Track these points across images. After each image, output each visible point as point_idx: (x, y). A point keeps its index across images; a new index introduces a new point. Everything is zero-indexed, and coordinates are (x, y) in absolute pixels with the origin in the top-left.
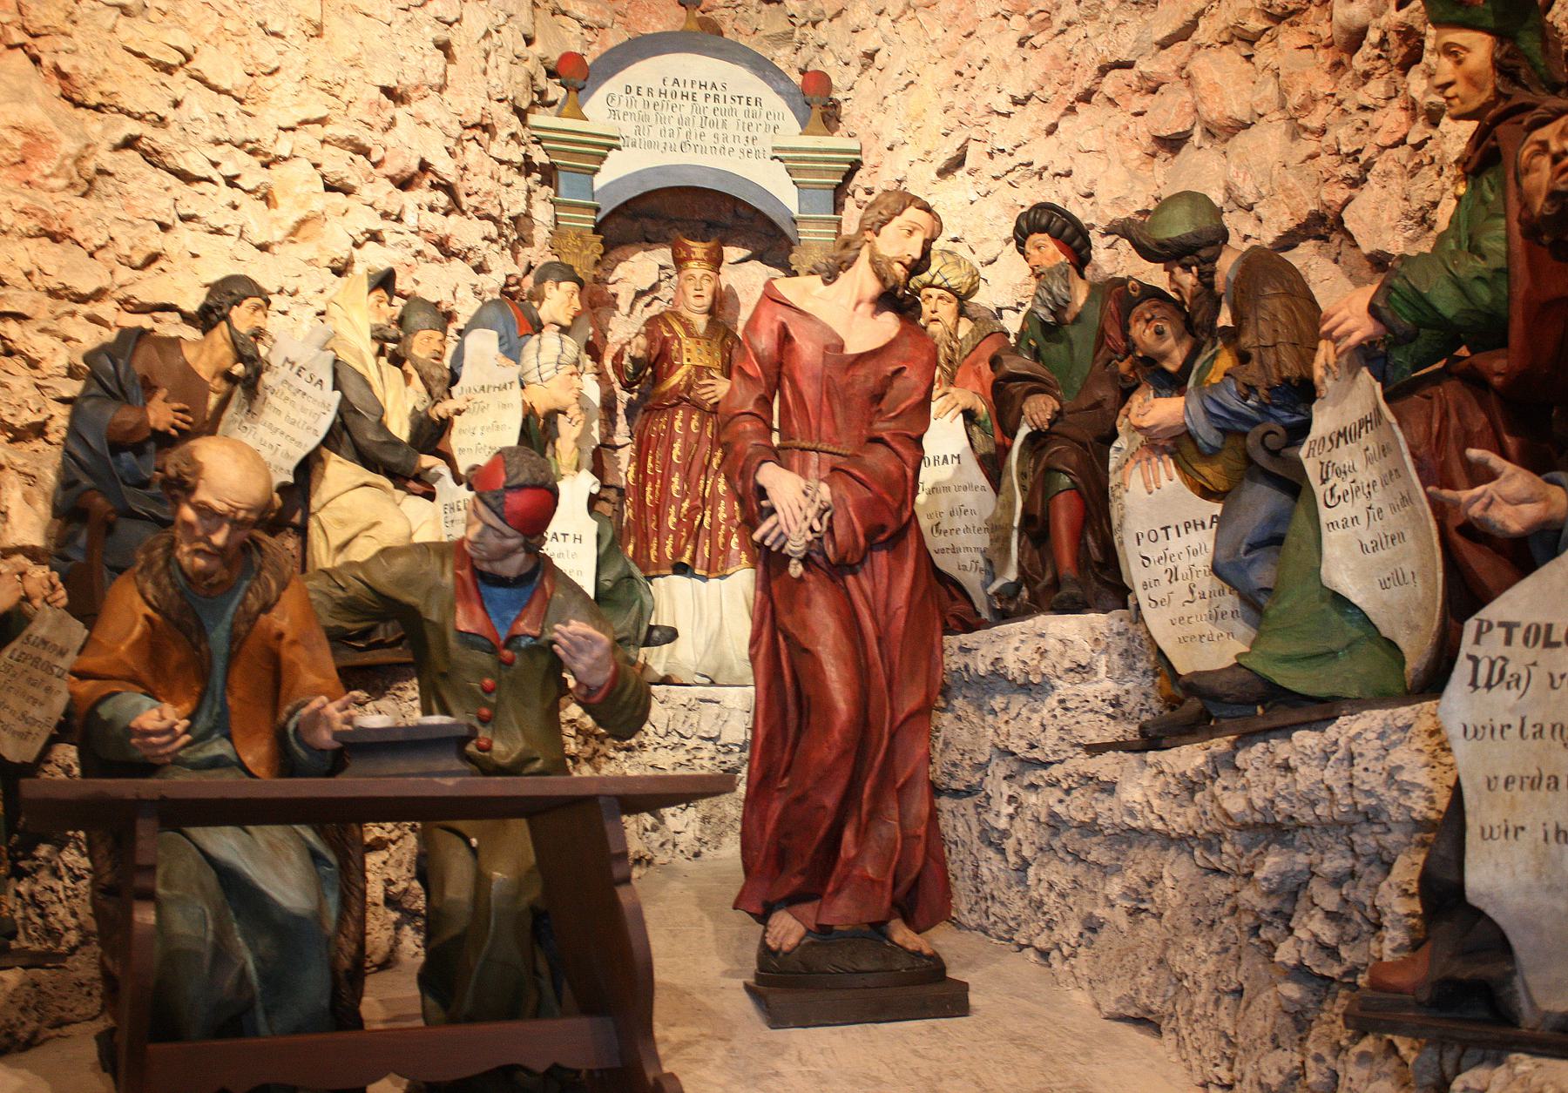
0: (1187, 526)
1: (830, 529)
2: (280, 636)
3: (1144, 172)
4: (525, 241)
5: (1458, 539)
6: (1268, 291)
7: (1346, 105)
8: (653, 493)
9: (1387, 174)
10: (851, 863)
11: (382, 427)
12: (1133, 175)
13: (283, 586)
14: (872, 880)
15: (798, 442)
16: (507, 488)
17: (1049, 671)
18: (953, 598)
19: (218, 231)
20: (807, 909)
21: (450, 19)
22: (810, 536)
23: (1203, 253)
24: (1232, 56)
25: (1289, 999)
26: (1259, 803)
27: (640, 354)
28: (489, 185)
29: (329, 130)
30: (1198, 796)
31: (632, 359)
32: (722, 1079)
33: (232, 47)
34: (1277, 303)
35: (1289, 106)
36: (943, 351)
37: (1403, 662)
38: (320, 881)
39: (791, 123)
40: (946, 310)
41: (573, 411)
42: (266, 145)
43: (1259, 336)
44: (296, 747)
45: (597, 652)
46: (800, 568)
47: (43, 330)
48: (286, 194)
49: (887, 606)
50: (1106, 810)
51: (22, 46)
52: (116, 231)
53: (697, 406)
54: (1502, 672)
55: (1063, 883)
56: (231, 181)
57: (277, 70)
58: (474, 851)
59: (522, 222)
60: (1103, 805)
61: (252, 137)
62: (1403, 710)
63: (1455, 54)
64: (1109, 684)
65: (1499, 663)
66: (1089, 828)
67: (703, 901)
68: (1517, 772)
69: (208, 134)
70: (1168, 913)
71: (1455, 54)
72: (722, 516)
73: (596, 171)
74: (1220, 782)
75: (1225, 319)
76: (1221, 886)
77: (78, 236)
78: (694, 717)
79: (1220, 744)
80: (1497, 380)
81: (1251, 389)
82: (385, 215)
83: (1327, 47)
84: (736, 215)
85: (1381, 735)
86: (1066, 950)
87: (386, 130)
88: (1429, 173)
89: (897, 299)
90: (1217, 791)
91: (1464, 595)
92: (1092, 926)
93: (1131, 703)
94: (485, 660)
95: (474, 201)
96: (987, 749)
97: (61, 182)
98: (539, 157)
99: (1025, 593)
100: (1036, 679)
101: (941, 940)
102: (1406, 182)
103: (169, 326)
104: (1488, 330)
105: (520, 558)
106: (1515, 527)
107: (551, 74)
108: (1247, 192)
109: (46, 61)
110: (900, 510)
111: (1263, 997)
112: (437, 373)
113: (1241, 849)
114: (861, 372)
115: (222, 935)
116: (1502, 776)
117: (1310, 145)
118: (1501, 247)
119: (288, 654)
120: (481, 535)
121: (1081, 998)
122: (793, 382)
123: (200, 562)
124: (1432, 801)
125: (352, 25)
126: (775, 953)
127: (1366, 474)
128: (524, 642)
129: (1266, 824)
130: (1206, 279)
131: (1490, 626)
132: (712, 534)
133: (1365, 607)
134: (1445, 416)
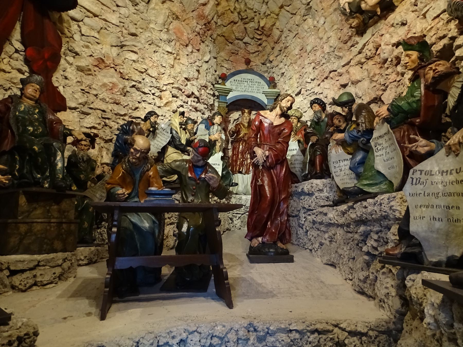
0: (344, 160)
2: (150, 176)
6: (364, 111)
7: (383, 75)
9: (391, 88)
10: (269, 229)
12: (336, 93)
13: (151, 166)
17: (313, 191)
19: (150, 104)
21: (200, 66)
23: (350, 104)
24: (358, 67)
25: (366, 260)
26: (359, 215)
28: (206, 98)
29: (174, 85)
30: (345, 215)
31: (232, 131)
33: (155, 69)
36: (294, 129)
37: (393, 186)
40: (295, 121)
41: (219, 140)
47: (113, 121)
48: (164, 97)
50: (325, 219)
51: (113, 67)
52: (129, 103)
54: (419, 181)
55: (315, 235)
56: (153, 94)
57: (164, 73)
59: (212, 105)
61: (158, 86)
62: (393, 193)
63: (409, 56)
64: (326, 194)
66: (321, 223)
68: (424, 204)
69: (149, 85)
70: (338, 241)
71: (409, 56)
74: (350, 211)
75: (354, 119)
76: (350, 235)
77: (122, 103)
79: (350, 204)
82: (184, 102)
84: (255, 105)
85: (388, 199)
86: (316, 249)
87: (185, 86)
89: (284, 115)
90: (349, 213)
91: (407, 168)
92: (321, 244)
93: (331, 198)
94: (193, 182)
95: (203, 101)
97: (119, 93)
98: (217, 94)
99: (309, 176)
101: (289, 247)
104: (416, 113)
105: (202, 162)
107: (220, 78)
108: (360, 94)
109: (118, 70)
111: (359, 259)
113: (354, 226)
117: (374, 84)
119: (151, 180)
121: (319, 260)
123: (134, 160)
124: (401, 213)
125: (180, 66)
126: (252, 247)
127: (385, 145)
130: (350, 110)
131: (416, 171)
133: (385, 174)
134: (404, 132)
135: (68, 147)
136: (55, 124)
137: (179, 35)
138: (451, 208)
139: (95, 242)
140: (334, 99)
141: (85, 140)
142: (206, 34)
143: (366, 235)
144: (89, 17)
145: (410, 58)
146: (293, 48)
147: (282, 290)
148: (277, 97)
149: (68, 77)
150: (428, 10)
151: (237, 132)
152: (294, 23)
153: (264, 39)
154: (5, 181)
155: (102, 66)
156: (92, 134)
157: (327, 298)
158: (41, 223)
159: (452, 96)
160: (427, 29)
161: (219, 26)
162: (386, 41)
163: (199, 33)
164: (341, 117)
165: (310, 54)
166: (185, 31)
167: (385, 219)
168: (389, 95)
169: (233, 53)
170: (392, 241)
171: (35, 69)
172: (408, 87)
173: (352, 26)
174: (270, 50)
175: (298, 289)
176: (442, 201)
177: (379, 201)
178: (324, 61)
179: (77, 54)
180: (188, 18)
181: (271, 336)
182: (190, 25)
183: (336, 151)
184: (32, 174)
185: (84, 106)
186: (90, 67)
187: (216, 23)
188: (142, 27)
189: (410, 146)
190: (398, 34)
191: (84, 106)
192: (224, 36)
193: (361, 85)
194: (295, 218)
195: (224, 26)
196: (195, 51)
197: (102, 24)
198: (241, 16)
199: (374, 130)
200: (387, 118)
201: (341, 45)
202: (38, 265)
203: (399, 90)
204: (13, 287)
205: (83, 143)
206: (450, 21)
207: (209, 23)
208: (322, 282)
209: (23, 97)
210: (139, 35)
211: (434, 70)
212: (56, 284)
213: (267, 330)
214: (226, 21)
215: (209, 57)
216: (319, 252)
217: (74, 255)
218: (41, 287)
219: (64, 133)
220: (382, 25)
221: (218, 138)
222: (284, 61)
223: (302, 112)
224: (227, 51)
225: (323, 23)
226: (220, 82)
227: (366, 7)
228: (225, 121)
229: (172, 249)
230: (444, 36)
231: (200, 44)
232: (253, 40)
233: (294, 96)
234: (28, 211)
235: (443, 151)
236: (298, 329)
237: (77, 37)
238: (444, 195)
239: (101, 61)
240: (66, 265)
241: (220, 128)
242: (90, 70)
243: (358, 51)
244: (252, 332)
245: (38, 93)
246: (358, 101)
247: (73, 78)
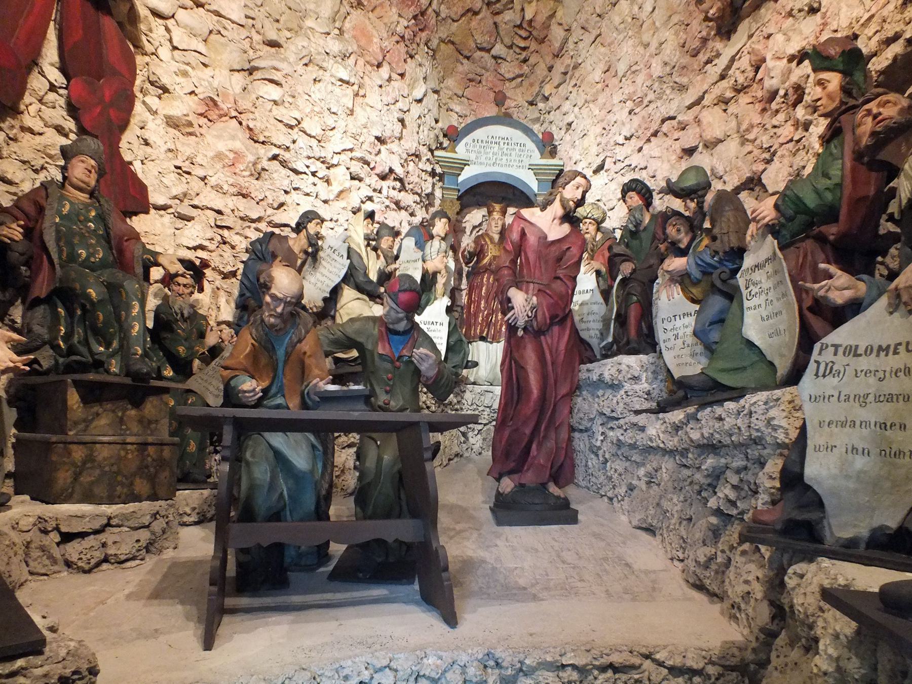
0: (684, 315)
1: (536, 316)
2: (305, 353)
4: (431, 204)
6: (727, 208)
9: (783, 156)
10: (534, 457)
11: (366, 275)
12: (672, 167)
13: (307, 332)
15: (526, 279)
17: (621, 379)
18: (586, 350)
19: (307, 194)
20: (516, 476)
21: (405, 110)
22: (527, 319)
23: (700, 193)
24: (718, 110)
25: (712, 524)
26: (706, 435)
27: (472, 250)
28: (417, 180)
29: (354, 154)
30: (680, 432)
32: (474, 547)
34: (730, 213)
35: (741, 130)
36: (590, 246)
38: (314, 457)
39: (537, 153)
40: (592, 228)
41: (443, 272)
42: (328, 159)
43: (721, 229)
44: (308, 400)
45: (431, 361)
47: (237, 234)
48: (335, 180)
49: (557, 350)
50: (641, 439)
51: (235, 117)
52: (267, 194)
55: (621, 469)
56: (314, 174)
58: (378, 446)
59: (430, 196)
61: (323, 155)
62: (776, 391)
64: (646, 385)
65: (830, 365)
66: (633, 446)
67: (480, 472)
68: (835, 418)
69: (305, 154)
70: (662, 484)
73: (459, 175)
74: (690, 426)
75: (707, 225)
76: (686, 472)
78: (483, 398)
79: (691, 410)
80: (832, 238)
81: (716, 252)
82: (375, 190)
83: (760, 102)
84: (514, 195)
85: (766, 403)
86: (620, 498)
87: (376, 155)
88: (802, 153)
89: (569, 218)
90: (688, 430)
91: (807, 340)
92: (631, 488)
93: (655, 394)
94: (388, 366)
95: (411, 186)
96: (595, 412)
97: (248, 173)
98: (439, 170)
99: (615, 347)
100: (616, 382)
101: (571, 492)
102: (791, 159)
103: (286, 232)
104: (830, 214)
106: (840, 301)
107: (445, 136)
108: (720, 170)
109: (244, 123)
110: (565, 308)
111: (701, 522)
112: (390, 255)
113: (696, 456)
114: (553, 249)
115: (273, 478)
116: (827, 421)
117: (749, 147)
118: (839, 173)
119: (308, 361)
120: (388, 312)
121: (624, 518)
123: (272, 320)
124: (787, 434)
125: (365, 110)
128: (405, 359)
129: (708, 445)
130: (700, 205)
131: (827, 346)
132: (495, 325)
133: (761, 347)
134: (805, 256)
135: (153, 289)
136: (126, 241)
137: (363, 43)
138: (888, 427)
139: (211, 480)
140: (668, 181)
141: (182, 275)
143: (717, 476)
144: (186, 9)
145: (824, 88)
146: (590, 68)
147: (552, 584)
148: (558, 176)
149: (150, 141)
151: (478, 253)
152: (592, 11)
153: (532, 49)
154: (23, 367)
155: (213, 115)
156: (198, 262)
157: (634, 599)
158: (109, 443)
160: (862, 21)
161: (443, 19)
162: (776, 49)
163: (403, 37)
164: (681, 221)
165: (624, 79)
166: (375, 33)
167: (756, 443)
169: (471, 80)
170: (766, 490)
171: (87, 125)
172: (819, 155)
173: (709, 15)
174: (546, 72)
175: (582, 580)
177: (747, 407)
178: (651, 96)
179: (165, 90)
181: (526, 675)
182: (386, 20)
184: (86, 343)
185: (182, 201)
186: (191, 118)
187: (438, 14)
188: (290, 26)
189: (816, 286)
190: (801, 33)
191: (182, 201)
192: (453, 43)
195: (453, 21)
196: (395, 76)
197: (211, 22)
199: (745, 251)
200: (773, 225)
201: (686, 60)
202: (108, 525)
203: (798, 161)
204: (68, 564)
205: (181, 280)
207: (423, 13)
208: (627, 565)
209: (67, 185)
210: (285, 45)
211: (875, 117)
212: (142, 560)
213: (519, 665)
215: (423, 90)
216: (626, 504)
217: (171, 506)
218: (116, 565)
219: (143, 260)
220: (770, 11)
221: (441, 266)
222: (572, 97)
223: (606, 208)
224: (459, 76)
225: (651, 9)
226: (445, 145)
228: (456, 230)
229: (351, 494)
231: (405, 61)
232: (512, 51)
233: (589, 173)
234: (85, 420)
235: (884, 301)
236: (576, 663)
237: (165, 52)
238: (878, 399)
239: (211, 103)
240: (158, 525)
241: (444, 244)
242: (190, 124)
243: (719, 72)
244: (492, 668)
245: (94, 176)
246: (717, 186)
247: (160, 142)
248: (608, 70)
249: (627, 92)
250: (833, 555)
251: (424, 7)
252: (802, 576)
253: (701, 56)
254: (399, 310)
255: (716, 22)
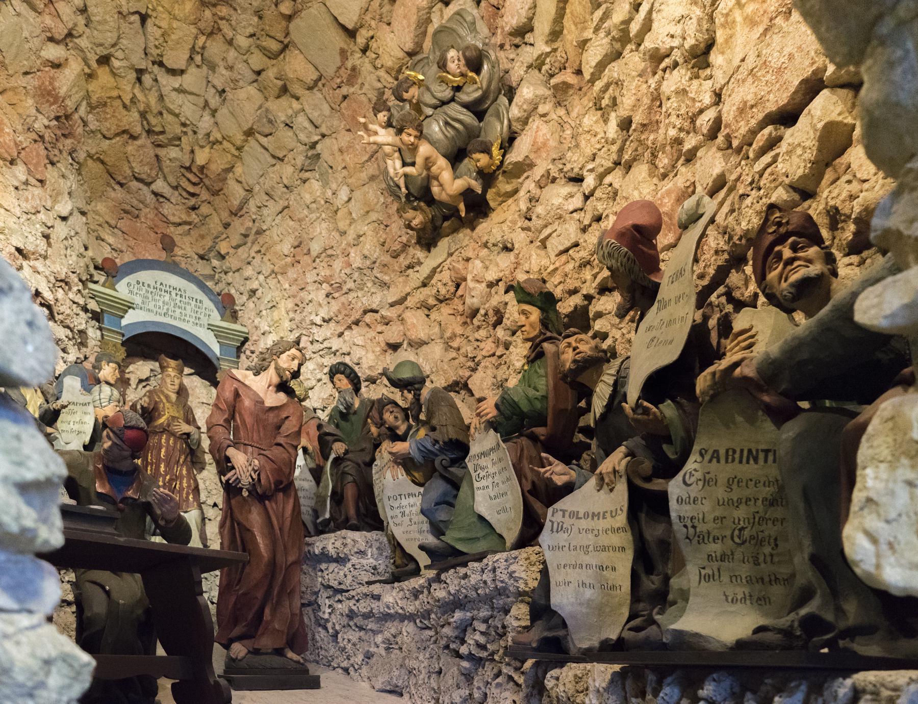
0: (409, 495)
1: (259, 479)
3: (382, 357)
5: (527, 494)
7: (470, 338)
8: (151, 470)
12: (377, 357)
14: (278, 631)
16: (125, 427)
17: (348, 552)
21: (49, 224)
23: (416, 386)
24: (421, 314)
25: (465, 668)
26: (453, 592)
31: (142, 407)
37: (505, 543)
46: (247, 493)
49: (283, 516)
53: (173, 434)
55: (354, 639)
60: (375, 605)
64: (371, 560)
66: (368, 616)
72: (185, 485)
73: (122, 317)
81: (436, 442)
86: (356, 667)
92: (368, 656)
93: (381, 569)
99: (332, 524)
100: (342, 556)
102: (495, 371)
106: (559, 483)
107: (96, 268)
113: (439, 615)
114: (271, 415)
122: (240, 414)
124: (526, 584)
130: (417, 398)
133: (490, 521)
134: (522, 450)
142: (60, 145)
143: (464, 628)
150: (550, 235)
152: (279, 180)
159: (599, 397)
160: (549, 270)
161: (92, 132)
162: (475, 272)
163: (42, 137)
165: (318, 260)
166: (6, 121)
168: (482, 380)
169: (126, 212)
170: (514, 629)
174: (221, 229)
176: (592, 559)
177: (490, 563)
180: (13, 89)
182: (21, 111)
183: (393, 477)
189: (542, 470)
190: (497, 265)
192: (103, 162)
193: (429, 351)
194: (308, 608)
196: (32, 181)
198: (148, 123)
201: (386, 258)
206: (585, 266)
207: (68, 117)
214: (110, 126)
216: (365, 671)
224: (111, 203)
225: (346, 199)
227: (440, 194)
230: (574, 292)
232: (176, 193)
235: (593, 481)
238: (596, 549)
248: (298, 246)
249: (323, 274)
250: (578, 660)
251: (70, 111)
252: (557, 679)
253: (401, 258)
254: (125, 447)
255: (418, 233)
